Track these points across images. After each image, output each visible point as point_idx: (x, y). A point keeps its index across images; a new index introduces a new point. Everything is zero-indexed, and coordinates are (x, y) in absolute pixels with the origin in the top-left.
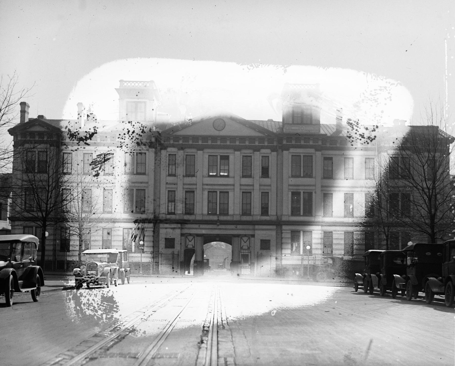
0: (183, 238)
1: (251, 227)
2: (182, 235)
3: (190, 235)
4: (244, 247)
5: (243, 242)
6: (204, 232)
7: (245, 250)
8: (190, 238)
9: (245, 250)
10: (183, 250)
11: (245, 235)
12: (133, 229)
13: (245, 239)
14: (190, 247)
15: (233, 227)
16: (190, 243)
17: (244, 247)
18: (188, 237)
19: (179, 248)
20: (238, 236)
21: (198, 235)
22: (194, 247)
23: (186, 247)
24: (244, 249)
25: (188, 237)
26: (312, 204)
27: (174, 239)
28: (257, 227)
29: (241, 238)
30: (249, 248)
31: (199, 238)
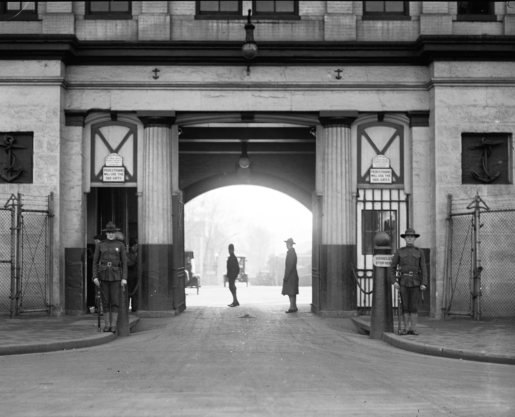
0: (77, 131)
1: (409, 75)
2: (72, 117)
3: (114, 117)
4: (376, 177)
5: (367, 151)
6: (310, 120)
7: (381, 187)
8: (115, 134)
9: (381, 187)
10: (76, 197)
11: (381, 117)
12: (46, 109)
13: (380, 135)
14: (113, 177)
15: (324, 74)
16: (114, 160)
17: (376, 177)
18: (104, 130)
19: (56, 182)
20: (345, 119)
21: (149, 119)
22: (134, 179)
23: (94, 178)
24: (374, 187)
25: (104, 130)
26: (90, 340)
27: (31, 134)
28: (441, 69)
29: (361, 132)
30: (398, 180)
31: (157, 133)
